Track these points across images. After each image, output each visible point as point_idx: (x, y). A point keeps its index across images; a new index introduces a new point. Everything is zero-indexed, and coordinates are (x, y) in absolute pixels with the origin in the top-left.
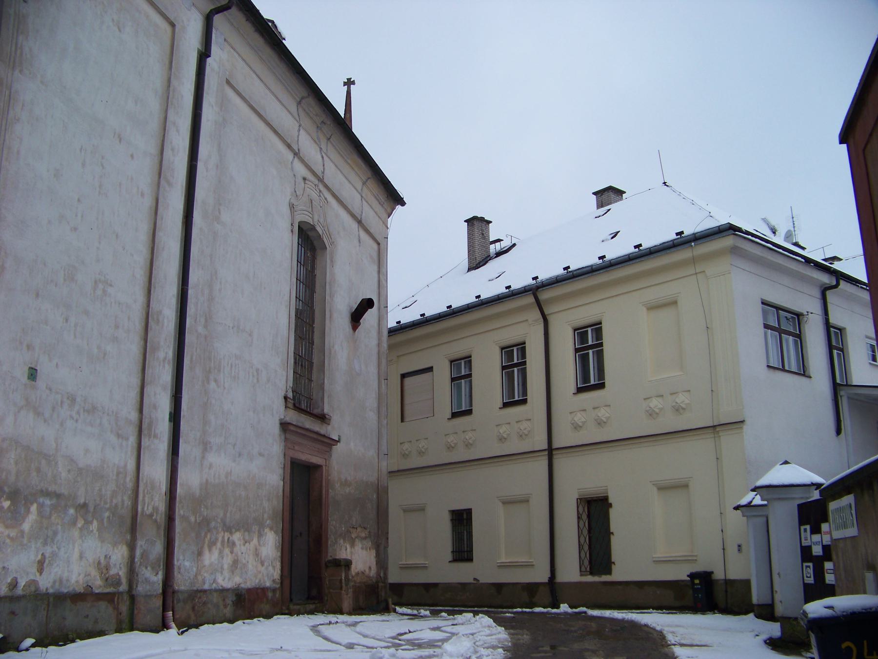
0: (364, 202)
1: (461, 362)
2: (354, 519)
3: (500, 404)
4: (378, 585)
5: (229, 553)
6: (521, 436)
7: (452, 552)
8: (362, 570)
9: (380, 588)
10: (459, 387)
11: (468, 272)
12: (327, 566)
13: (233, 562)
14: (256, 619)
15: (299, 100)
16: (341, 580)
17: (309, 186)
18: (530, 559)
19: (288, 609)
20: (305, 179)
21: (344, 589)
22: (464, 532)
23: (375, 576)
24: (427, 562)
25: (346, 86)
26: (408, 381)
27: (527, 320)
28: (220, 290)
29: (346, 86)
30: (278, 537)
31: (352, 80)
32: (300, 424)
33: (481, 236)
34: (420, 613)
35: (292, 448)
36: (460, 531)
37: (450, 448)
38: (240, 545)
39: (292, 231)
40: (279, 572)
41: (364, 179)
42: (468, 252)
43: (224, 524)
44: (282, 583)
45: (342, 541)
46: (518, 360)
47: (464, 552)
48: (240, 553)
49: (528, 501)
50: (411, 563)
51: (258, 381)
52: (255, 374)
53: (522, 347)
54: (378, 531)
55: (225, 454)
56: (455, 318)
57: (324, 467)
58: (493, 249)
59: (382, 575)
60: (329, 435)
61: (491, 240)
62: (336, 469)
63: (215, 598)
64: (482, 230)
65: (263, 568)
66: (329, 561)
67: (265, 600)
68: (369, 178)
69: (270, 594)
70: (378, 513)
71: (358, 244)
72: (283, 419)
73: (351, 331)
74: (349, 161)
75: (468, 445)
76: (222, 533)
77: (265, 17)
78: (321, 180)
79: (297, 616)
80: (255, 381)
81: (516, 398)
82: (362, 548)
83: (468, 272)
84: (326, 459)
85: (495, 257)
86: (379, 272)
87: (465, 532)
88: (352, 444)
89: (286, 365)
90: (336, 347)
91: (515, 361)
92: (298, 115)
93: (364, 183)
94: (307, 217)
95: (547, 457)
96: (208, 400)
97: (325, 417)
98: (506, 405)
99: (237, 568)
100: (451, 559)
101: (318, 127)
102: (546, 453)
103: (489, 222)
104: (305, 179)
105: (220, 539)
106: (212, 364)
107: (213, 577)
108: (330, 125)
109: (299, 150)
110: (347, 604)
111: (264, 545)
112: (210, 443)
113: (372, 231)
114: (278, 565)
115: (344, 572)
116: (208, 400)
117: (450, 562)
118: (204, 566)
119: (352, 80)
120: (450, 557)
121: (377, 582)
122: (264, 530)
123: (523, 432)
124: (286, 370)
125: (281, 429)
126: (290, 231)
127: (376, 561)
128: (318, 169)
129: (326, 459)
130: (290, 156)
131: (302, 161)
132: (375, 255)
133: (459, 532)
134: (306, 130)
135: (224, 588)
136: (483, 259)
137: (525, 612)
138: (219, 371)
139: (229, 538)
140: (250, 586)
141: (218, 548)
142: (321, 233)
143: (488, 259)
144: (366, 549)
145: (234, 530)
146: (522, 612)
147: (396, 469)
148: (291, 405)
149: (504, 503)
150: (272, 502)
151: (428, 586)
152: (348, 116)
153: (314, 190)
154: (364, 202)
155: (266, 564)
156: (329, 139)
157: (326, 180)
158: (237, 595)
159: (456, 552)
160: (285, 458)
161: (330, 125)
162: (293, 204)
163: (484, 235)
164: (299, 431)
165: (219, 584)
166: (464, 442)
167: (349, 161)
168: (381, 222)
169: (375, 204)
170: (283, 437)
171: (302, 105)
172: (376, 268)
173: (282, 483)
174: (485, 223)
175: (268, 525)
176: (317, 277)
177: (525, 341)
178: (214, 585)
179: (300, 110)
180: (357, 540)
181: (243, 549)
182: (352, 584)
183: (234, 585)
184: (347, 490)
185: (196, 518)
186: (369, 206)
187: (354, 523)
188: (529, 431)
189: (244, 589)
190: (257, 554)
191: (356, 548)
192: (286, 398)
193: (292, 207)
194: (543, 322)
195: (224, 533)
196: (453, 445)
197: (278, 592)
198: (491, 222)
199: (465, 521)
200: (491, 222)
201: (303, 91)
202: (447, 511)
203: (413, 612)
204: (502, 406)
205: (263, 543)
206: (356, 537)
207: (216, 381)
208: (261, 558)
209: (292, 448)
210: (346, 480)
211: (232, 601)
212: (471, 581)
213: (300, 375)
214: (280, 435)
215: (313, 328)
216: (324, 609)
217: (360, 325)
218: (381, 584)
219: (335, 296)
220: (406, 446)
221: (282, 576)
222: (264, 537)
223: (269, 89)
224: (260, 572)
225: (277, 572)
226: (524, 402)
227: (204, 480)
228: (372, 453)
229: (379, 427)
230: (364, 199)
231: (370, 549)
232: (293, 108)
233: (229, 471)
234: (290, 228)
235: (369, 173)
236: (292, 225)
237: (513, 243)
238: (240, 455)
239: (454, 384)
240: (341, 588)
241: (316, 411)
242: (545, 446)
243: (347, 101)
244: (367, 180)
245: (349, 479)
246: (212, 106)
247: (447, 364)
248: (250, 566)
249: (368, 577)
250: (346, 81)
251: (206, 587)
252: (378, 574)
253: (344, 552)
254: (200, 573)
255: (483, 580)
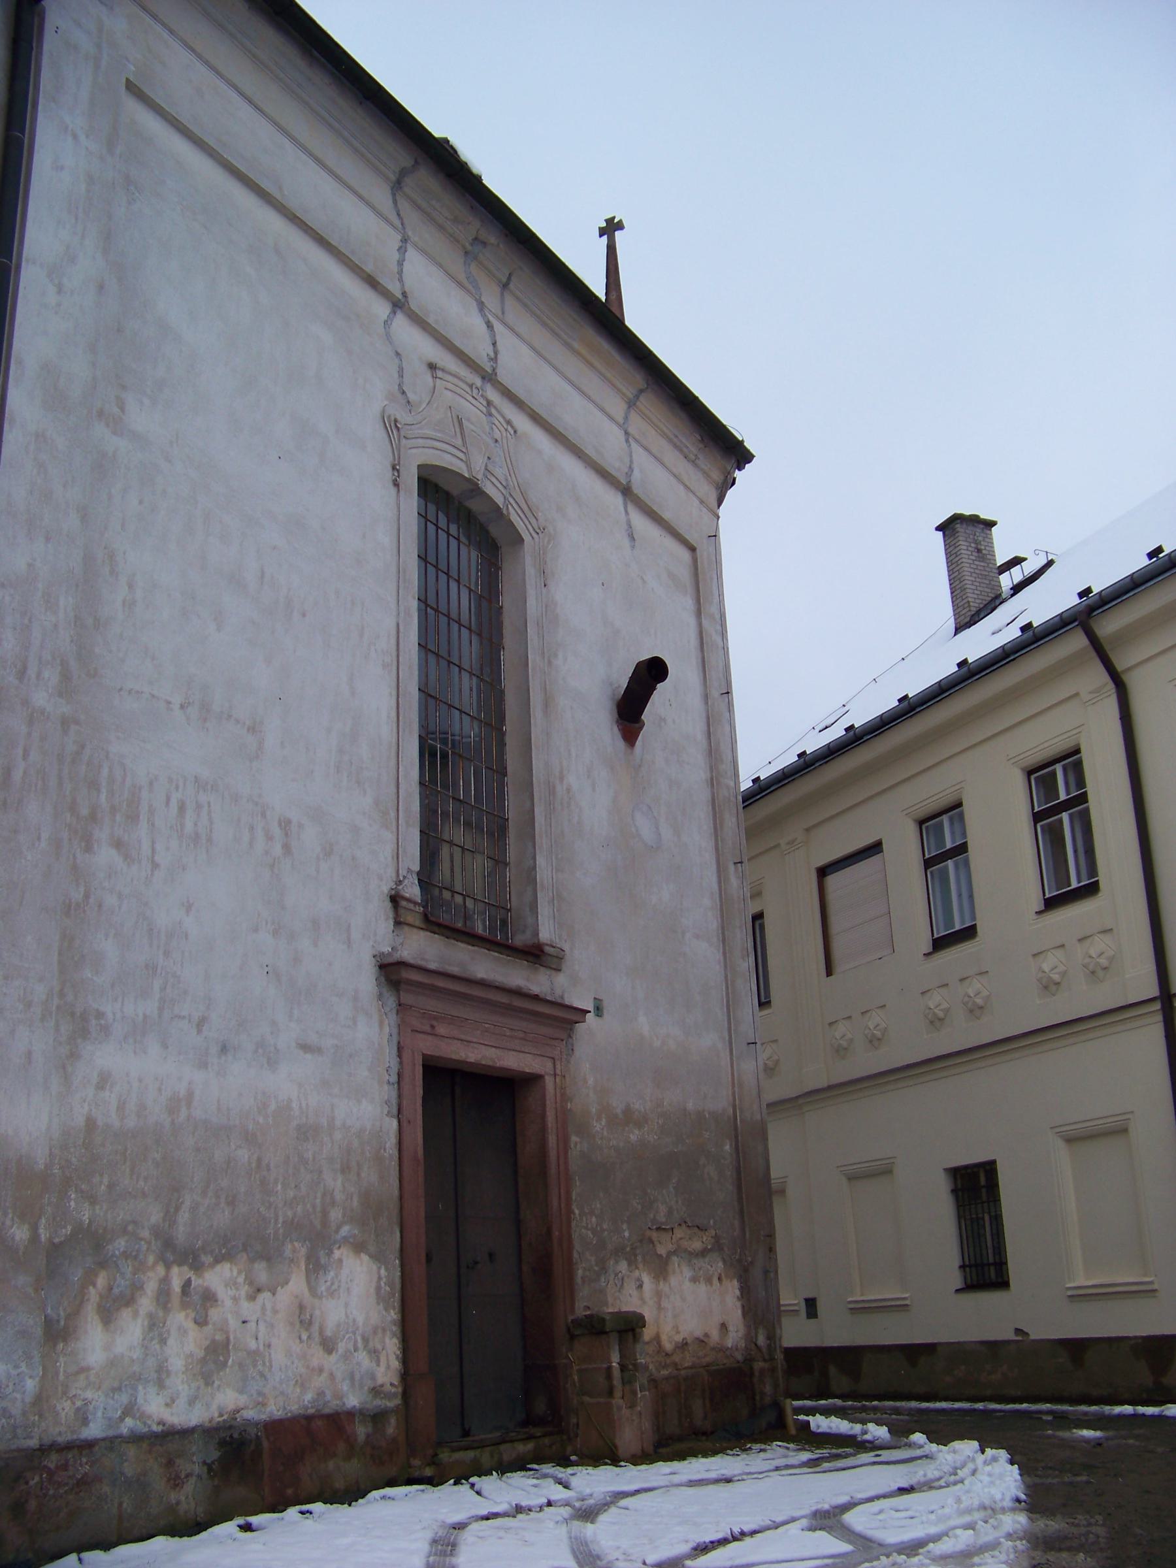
0: (634, 445)
1: (942, 821)
2: (663, 1209)
3: (1037, 903)
4: (751, 1368)
5: (190, 1325)
6: (1093, 973)
7: (960, 1267)
8: (699, 1333)
9: (757, 1374)
10: (944, 878)
11: (955, 635)
12: (572, 1337)
13: (207, 1349)
14: (298, 1508)
15: (393, 178)
16: (609, 1368)
17: (450, 386)
18: (1145, 1275)
19: (433, 1461)
20: (432, 367)
21: (618, 1393)
22: (983, 1219)
23: (742, 1344)
24: (907, 1295)
25: (606, 236)
26: (832, 881)
27: (1077, 694)
28: (129, 605)
29: (606, 236)
30: (387, 1269)
31: (616, 221)
32: (455, 970)
33: (975, 554)
34: (865, 1432)
35: (427, 1028)
36: (974, 1216)
37: (936, 1022)
38: (235, 1299)
39: (396, 484)
40: (396, 1364)
41: (630, 393)
42: (952, 593)
43: (168, 1244)
44: (405, 1395)
45: (623, 1266)
46: (1068, 794)
47: (989, 1265)
48: (233, 1323)
49: (1125, 1131)
50: (873, 1298)
51: (287, 849)
52: (277, 831)
53: (1072, 758)
54: (743, 1230)
55: (165, 1046)
56: (914, 718)
57: (549, 1082)
58: (1006, 581)
59: (761, 1340)
60: (562, 997)
61: (999, 563)
62: (591, 1081)
63: (131, 1463)
64: (977, 542)
65: (333, 1358)
66: (577, 1323)
67: (341, 1447)
68: (641, 391)
69: (361, 1431)
70: (739, 1188)
71: (626, 542)
72: (389, 954)
73: (621, 744)
74: (576, 345)
75: (975, 1010)
76: (161, 1270)
77: (436, 135)
78: (489, 377)
79: (455, 1484)
80: (278, 850)
81: (1074, 884)
82: (694, 1280)
83: (955, 635)
84: (553, 1058)
85: (1012, 595)
86: (699, 613)
87: (987, 1217)
88: (642, 1019)
89: (393, 814)
90: (571, 779)
91: (1063, 796)
92: (398, 215)
93: (631, 404)
94: (454, 460)
95: (1159, 1017)
96: (87, 896)
97: (542, 951)
98: (1051, 904)
99: (225, 1364)
100: (959, 1284)
101: (466, 253)
102: (1157, 1006)
103: (991, 524)
104: (432, 367)
105: (151, 1286)
106: (103, 797)
107: (124, 1398)
108: (498, 245)
109: (404, 294)
110: (628, 1437)
111: (332, 1294)
112: (100, 1015)
113: (667, 515)
114: (391, 1346)
115: (617, 1347)
116: (87, 896)
117: (957, 1291)
118: (85, 1370)
119: (616, 221)
120: (957, 1281)
121: (749, 1360)
122: (330, 1252)
123: (1098, 962)
124: (395, 830)
125: (383, 979)
126: (391, 485)
127: (743, 1307)
128: (480, 350)
129: (553, 1058)
130: (382, 309)
131: (419, 321)
132: (685, 575)
133: (972, 1219)
134: (423, 252)
135: (172, 1426)
136: (985, 603)
137: (1143, 1415)
138: (133, 818)
139: (189, 1282)
140: (279, 1414)
141: (143, 1311)
142: (499, 501)
143: (998, 602)
144: (709, 1281)
145: (207, 1259)
146: (1135, 1416)
147: (823, 1083)
148: (415, 919)
149: (1070, 1140)
150: (358, 1175)
151: (914, 1352)
152: (613, 296)
153: (470, 398)
154: (634, 445)
155: (342, 1347)
156: (505, 286)
157: (503, 377)
158: (222, 1443)
159: (970, 1266)
160: (400, 1056)
161: (498, 245)
162: (396, 421)
163: (983, 553)
164: (441, 983)
165: (150, 1417)
166: (965, 1004)
167: (576, 345)
168: (695, 499)
169: (671, 456)
170: (391, 1002)
171: (406, 189)
172: (689, 602)
173: (395, 1123)
174: (982, 526)
175: (345, 1238)
176: (505, 610)
177: (1078, 745)
178: (129, 1422)
179: (404, 205)
180: (675, 1259)
181: (248, 1309)
182: (642, 1379)
183: (216, 1415)
184: (634, 1136)
185: (34, 1229)
186: (652, 459)
187: (661, 1218)
188: (1111, 959)
189: (257, 1424)
190: (303, 1319)
191: (674, 1280)
192: (395, 899)
193: (392, 426)
194: (1114, 691)
195: (168, 1267)
196: (941, 1015)
197: (393, 1421)
198: (994, 524)
199: (984, 1190)
200: (994, 524)
201: (399, 155)
202: (942, 1171)
203: (852, 1428)
204: (1043, 908)
205: (328, 1289)
206: (670, 1254)
207: (118, 844)
208: (321, 1331)
209: (427, 1028)
210: (628, 1111)
211: (204, 1463)
212: (1011, 1336)
213: (462, 848)
214: (380, 997)
215: (503, 734)
216: (569, 1449)
217: (641, 728)
218: (759, 1365)
219: (560, 656)
220: (841, 1028)
221: (406, 1375)
222: (332, 1274)
223: (589, 398)
224: (321, 1370)
225: (388, 1367)
226: (1092, 889)
227: (80, 1121)
228: (710, 1040)
229: (726, 977)
230: (636, 440)
231: (720, 1279)
232: (381, 195)
233: (183, 1093)
234: (389, 475)
235: (639, 378)
236: (394, 468)
237: (1049, 559)
238: (224, 1049)
239: (931, 873)
240: (610, 1392)
241: (519, 940)
242: (1153, 990)
243: (611, 266)
244: (637, 397)
245: (637, 1106)
246: (75, 137)
247: (911, 830)
248: (278, 1356)
249: (721, 1349)
250: (604, 225)
251: (94, 1430)
252: (750, 1338)
253: (635, 1293)
254: (65, 1393)
255: (1037, 1333)
